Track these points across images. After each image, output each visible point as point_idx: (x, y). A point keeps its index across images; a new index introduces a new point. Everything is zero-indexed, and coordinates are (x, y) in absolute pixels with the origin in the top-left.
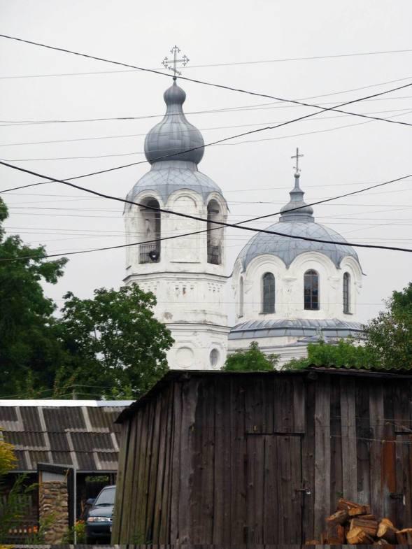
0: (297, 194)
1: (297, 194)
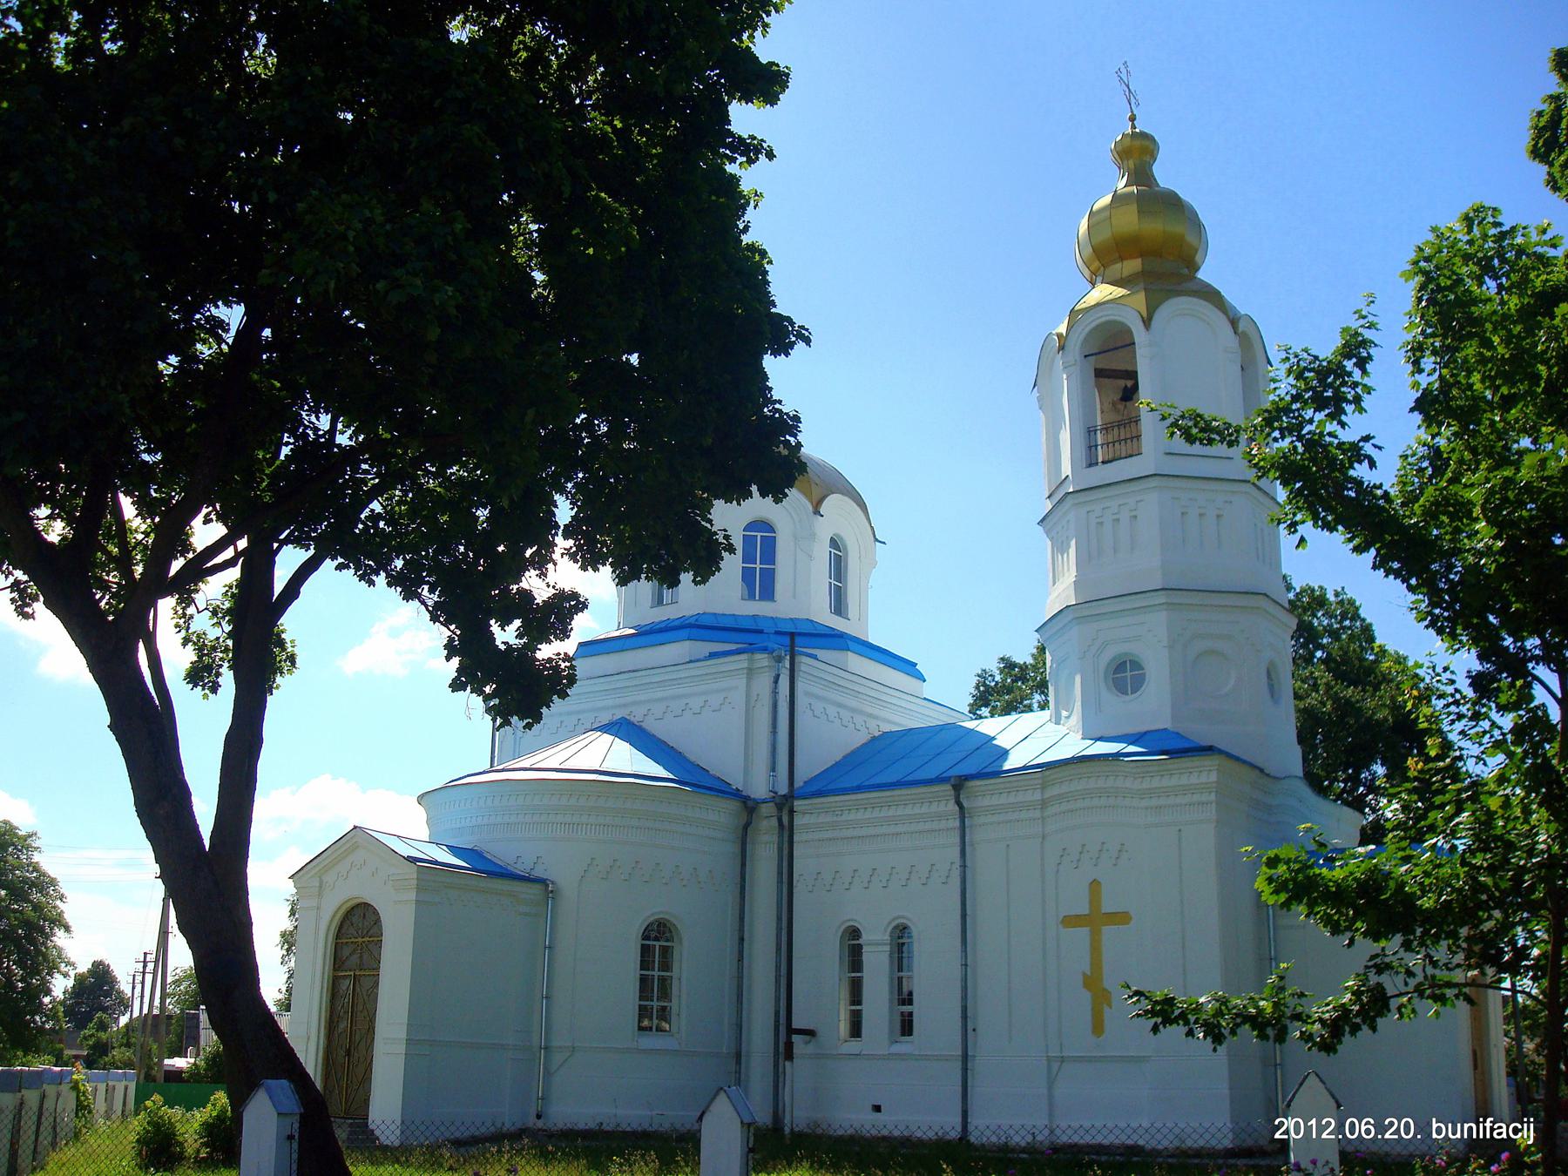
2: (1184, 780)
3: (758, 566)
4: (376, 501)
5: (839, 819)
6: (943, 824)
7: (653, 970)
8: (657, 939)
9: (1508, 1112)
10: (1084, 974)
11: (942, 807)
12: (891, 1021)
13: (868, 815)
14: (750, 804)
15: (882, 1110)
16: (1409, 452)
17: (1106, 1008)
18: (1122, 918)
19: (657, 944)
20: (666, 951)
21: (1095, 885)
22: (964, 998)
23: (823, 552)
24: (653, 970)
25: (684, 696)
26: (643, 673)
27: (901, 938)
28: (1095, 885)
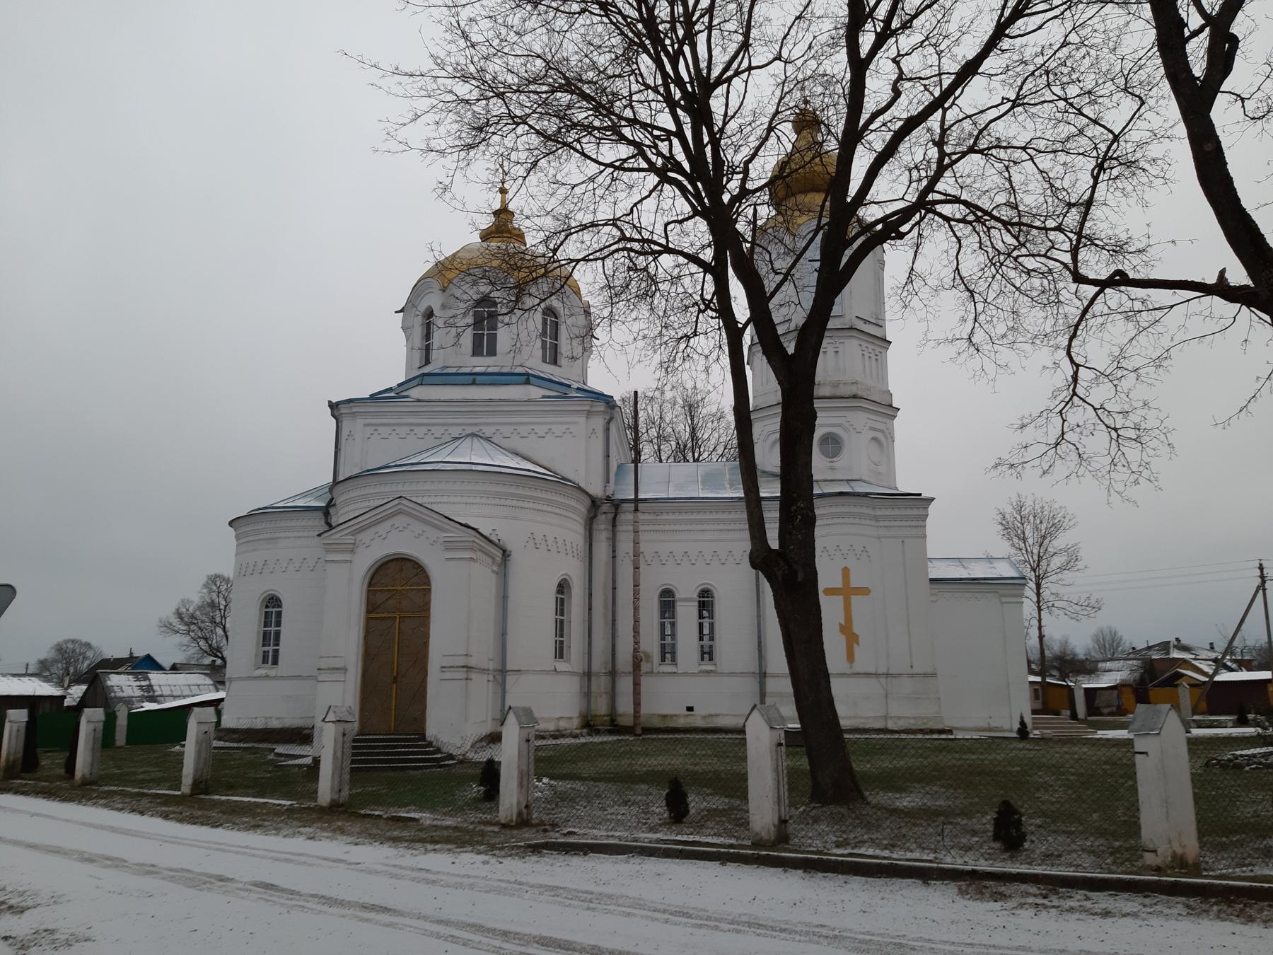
0: (503, 213)
1: (503, 213)
2: (903, 512)
3: (486, 332)
4: (819, 258)
5: (659, 517)
6: (737, 527)
7: (271, 626)
8: (274, 607)
9: (192, 771)
10: (840, 624)
11: (737, 516)
12: (256, 655)
13: (711, 517)
14: (615, 502)
15: (691, 705)
16: (983, 266)
17: (855, 646)
18: (865, 591)
19: (274, 610)
20: (279, 614)
21: (846, 572)
22: (759, 637)
23: (858, 320)
24: (271, 626)
25: (567, 423)
26: (425, 403)
27: (705, 601)
28: (846, 572)
